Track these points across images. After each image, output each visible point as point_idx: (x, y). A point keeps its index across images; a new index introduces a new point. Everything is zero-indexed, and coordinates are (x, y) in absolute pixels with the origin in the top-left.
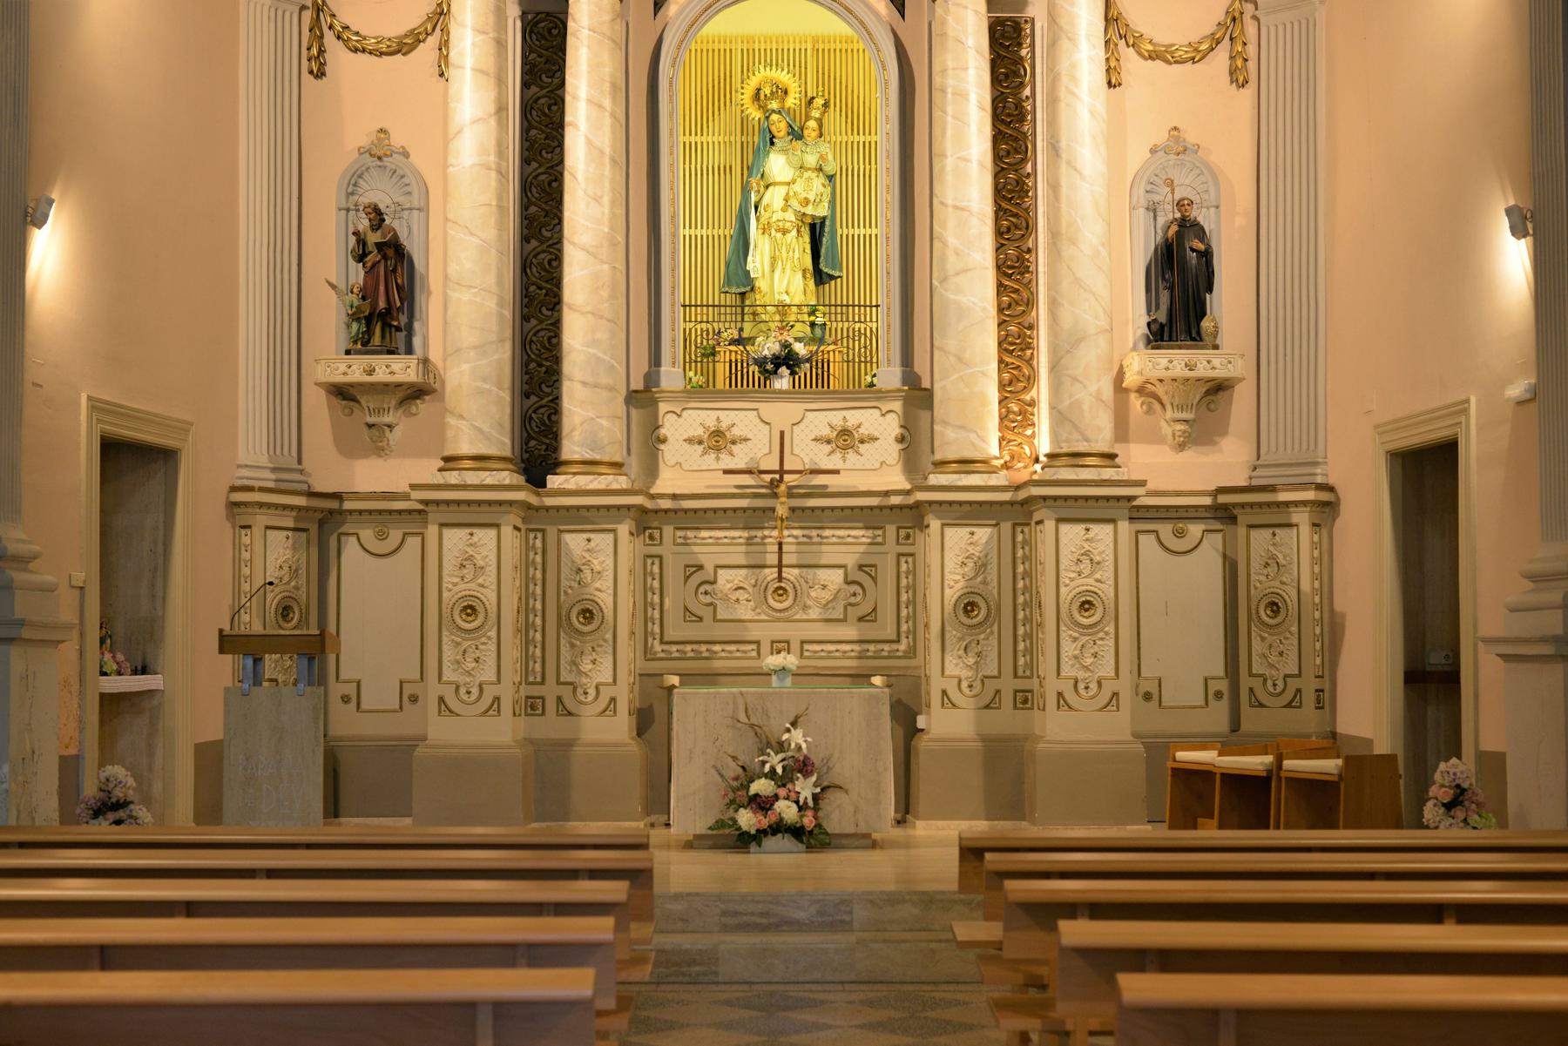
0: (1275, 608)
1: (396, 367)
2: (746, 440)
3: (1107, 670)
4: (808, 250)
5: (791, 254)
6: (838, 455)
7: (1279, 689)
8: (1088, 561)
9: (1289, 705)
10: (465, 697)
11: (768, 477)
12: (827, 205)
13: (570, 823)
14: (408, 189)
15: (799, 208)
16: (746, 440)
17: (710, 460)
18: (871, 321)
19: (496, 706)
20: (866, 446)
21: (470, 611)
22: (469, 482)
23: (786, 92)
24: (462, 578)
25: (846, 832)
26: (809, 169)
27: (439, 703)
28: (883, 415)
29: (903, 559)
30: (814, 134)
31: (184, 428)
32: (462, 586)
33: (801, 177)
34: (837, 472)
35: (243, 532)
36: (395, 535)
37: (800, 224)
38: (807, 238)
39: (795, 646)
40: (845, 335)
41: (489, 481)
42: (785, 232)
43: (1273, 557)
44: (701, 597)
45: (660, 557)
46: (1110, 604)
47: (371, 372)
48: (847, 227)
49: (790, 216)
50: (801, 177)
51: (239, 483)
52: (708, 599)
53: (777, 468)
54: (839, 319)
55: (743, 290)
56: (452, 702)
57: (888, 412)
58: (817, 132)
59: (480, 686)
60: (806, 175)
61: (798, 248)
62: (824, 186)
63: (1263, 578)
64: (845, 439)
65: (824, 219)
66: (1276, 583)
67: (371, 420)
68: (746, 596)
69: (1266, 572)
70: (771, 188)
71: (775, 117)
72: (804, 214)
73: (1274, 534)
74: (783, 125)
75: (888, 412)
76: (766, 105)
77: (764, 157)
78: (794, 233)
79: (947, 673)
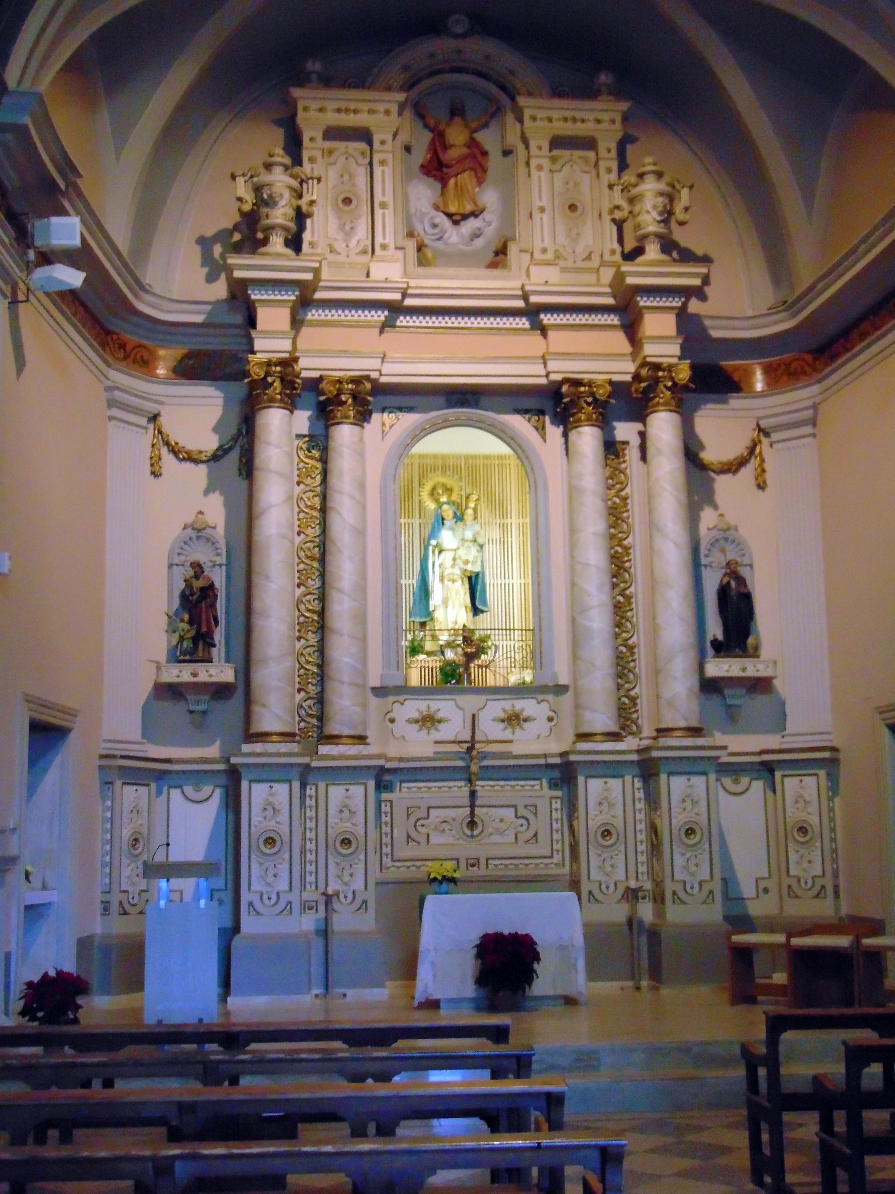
0: (804, 830)
4: (468, 594)
6: (509, 730)
8: (690, 801)
10: (803, 885)
14: (219, 551)
15: (462, 566)
18: (510, 640)
19: (288, 907)
20: (528, 723)
21: (346, 842)
22: (270, 751)
24: (684, 809)
25: (548, 994)
27: (249, 906)
28: (538, 703)
29: (554, 801)
30: (471, 518)
31: (72, 713)
33: (463, 546)
34: (511, 742)
35: (107, 786)
38: (467, 586)
39: (483, 862)
40: (509, 650)
42: (453, 581)
43: (801, 796)
45: (391, 802)
46: (286, 838)
47: (195, 675)
49: (457, 571)
50: (463, 546)
53: (469, 739)
54: (501, 638)
55: (423, 620)
57: (542, 701)
59: (278, 893)
60: (467, 544)
61: (460, 593)
63: (794, 810)
64: (513, 719)
66: (273, 823)
67: (192, 708)
68: (449, 827)
69: (340, 817)
71: (445, 507)
72: (466, 570)
73: (271, 787)
74: (451, 513)
75: (542, 701)
76: (439, 499)
79: (253, 888)
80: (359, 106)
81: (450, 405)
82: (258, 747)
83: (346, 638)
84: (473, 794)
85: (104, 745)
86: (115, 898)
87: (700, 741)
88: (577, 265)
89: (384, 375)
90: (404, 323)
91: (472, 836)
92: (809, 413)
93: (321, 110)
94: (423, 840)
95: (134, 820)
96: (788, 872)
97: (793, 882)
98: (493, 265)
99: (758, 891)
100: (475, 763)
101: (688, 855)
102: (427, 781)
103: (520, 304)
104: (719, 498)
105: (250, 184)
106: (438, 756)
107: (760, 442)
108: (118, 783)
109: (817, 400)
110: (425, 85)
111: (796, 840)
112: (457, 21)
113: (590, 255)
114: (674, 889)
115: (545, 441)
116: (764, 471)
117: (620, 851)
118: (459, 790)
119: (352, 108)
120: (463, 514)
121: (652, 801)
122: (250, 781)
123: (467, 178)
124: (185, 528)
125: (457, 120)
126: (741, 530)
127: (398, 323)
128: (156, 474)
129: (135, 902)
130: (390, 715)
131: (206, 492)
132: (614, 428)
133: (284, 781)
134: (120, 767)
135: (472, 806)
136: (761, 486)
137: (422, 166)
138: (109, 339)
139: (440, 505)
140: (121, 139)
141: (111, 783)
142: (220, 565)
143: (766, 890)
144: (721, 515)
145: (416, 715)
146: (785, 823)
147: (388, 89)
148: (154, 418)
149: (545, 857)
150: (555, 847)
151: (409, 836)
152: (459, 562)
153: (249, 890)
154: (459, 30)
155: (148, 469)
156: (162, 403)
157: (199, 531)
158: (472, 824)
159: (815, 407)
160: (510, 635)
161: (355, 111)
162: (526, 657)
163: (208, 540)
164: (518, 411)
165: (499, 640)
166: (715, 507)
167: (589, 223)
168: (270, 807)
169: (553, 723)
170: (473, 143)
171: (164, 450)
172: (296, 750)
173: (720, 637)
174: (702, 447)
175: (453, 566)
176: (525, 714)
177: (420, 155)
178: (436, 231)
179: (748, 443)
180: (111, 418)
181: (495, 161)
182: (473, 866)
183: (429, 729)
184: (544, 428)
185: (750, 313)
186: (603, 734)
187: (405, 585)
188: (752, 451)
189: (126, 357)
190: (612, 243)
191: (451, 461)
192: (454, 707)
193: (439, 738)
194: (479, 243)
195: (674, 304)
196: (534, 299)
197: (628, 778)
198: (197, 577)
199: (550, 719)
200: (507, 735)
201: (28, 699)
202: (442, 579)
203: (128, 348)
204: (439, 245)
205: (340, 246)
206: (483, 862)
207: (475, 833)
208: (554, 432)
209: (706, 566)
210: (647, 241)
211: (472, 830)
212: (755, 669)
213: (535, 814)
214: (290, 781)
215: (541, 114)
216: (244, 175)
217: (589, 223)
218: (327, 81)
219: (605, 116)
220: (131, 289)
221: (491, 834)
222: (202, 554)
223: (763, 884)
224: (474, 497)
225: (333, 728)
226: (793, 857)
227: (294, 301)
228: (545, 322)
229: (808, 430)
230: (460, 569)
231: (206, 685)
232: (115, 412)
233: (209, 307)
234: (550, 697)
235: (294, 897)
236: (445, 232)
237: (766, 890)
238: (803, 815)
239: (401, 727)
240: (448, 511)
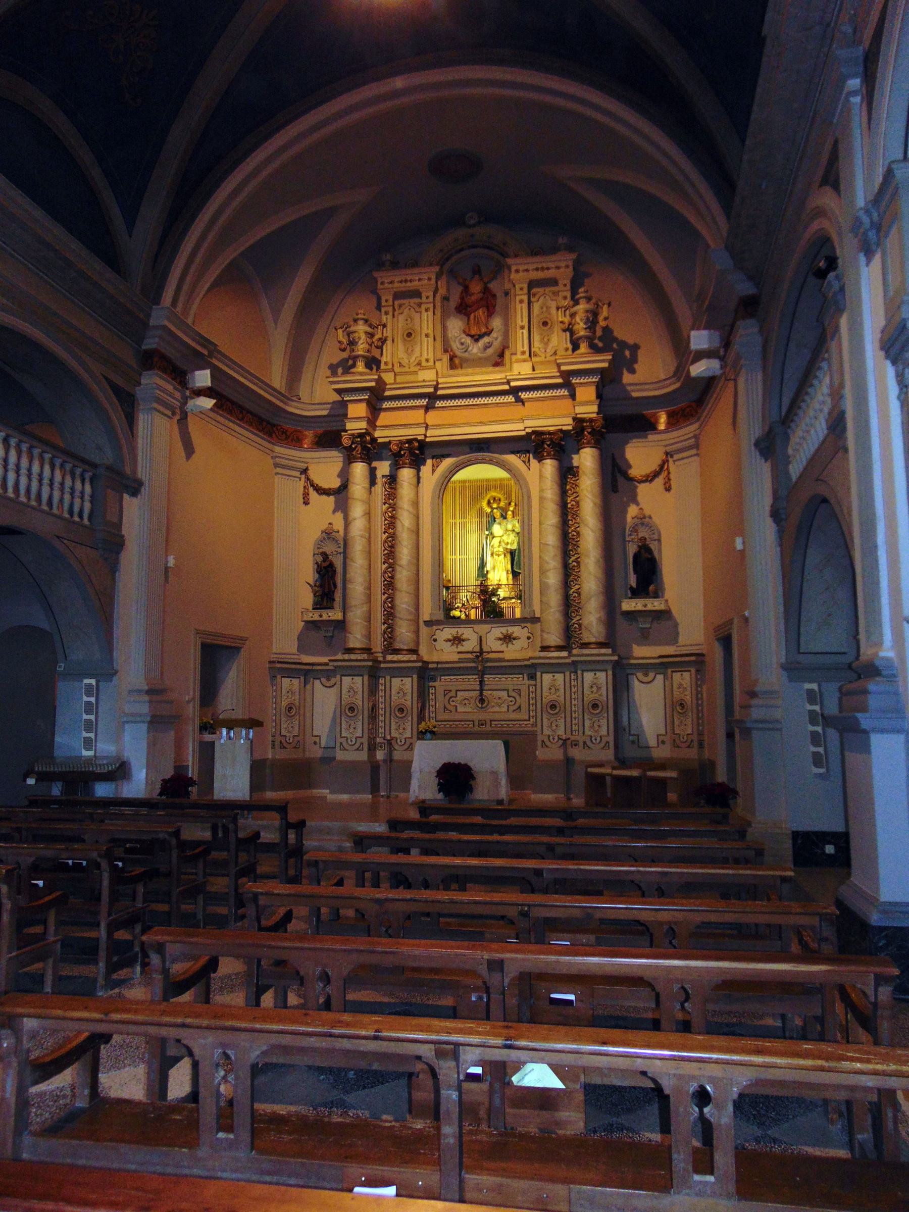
1: (656, 604)
2: (469, 640)
3: (604, 731)
6: (505, 645)
7: (354, 742)
9: (357, 749)
10: (350, 743)
11: (475, 654)
13: (314, 791)
16: (469, 640)
17: (454, 648)
21: (553, 707)
23: (500, 500)
32: (591, 696)
36: (651, 675)
41: (359, 658)
42: (499, 555)
43: (352, 688)
44: (452, 703)
45: (435, 687)
46: (409, 709)
47: (645, 606)
49: (501, 549)
51: (272, 660)
52: (454, 704)
56: (589, 743)
64: (508, 639)
65: (515, 550)
71: (495, 511)
73: (595, 674)
78: (503, 556)
80: (413, 277)
81: (472, 451)
82: (396, 657)
83: (404, 594)
84: (481, 682)
85: (272, 656)
86: (278, 739)
88: (547, 359)
90: (440, 405)
91: (482, 708)
92: (692, 441)
93: (391, 283)
94: (453, 710)
95: (290, 696)
96: (341, 733)
98: (496, 364)
99: (658, 743)
101: (552, 719)
102: (462, 675)
103: (506, 387)
104: (640, 498)
105: (345, 333)
106: (461, 661)
107: (668, 461)
108: (279, 677)
109: (697, 432)
110: (454, 259)
111: (397, 716)
112: (471, 217)
113: (555, 352)
116: (669, 479)
118: (472, 681)
119: (409, 279)
120: (506, 514)
121: (373, 690)
122: (542, 673)
123: (481, 313)
125: (477, 276)
126: (654, 519)
127: (436, 406)
128: (306, 503)
129: (291, 741)
130: (434, 637)
131: (334, 512)
132: (572, 459)
133: (603, 670)
134: (279, 668)
135: (481, 690)
136: (668, 489)
137: (456, 308)
138: (275, 429)
139: (493, 509)
140: (276, 313)
141: (276, 677)
142: (340, 553)
143: (663, 742)
144: (641, 509)
145: (450, 637)
147: (431, 265)
148: (305, 471)
149: (525, 720)
150: (531, 714)
151: (445, 708)
152: (503, 544)
153: (584, 733)
154: (472, 222)
155: (302, 501)
156: (307, 463)
157: (329, 534)
158: (482, 701)
159: (695, 436)
161: (411, 281)
163: (334, 539)
164: (513, 453)
166: (637, 504)
167: (555, 333)
168: (553, 687)
169: (531, 640)
170: (486, 290)
171: (311, 489)
173: (634, 585)
174: (630, 467)
175: (499, 546)
177: (454, 302)
178: (464, 347)
179: (659, 462)
180: (277, 474)
181: (500, 300)
182: (482, 725)
183: (507, 644)
184: (529, 461)
185: (664, 377)
186: (407, 650)
188: (661, 467)
189: (286, 439)
190: (566, 344)
191: (506, 482)
192: (472, 632)
194: (490, 351)
195: (594, 380)
196: (513, 384)
197: (567, 674)
198: (324, 561)
199: (435, 640)
200: (503, 648)
201: (198, 632)
202: (492, 555)
203: (288, 433)
204: (466, 355)
205: (405, 362)
206: (488, 722)
207: (484, 705)
208: (534, 462)
209: (629, 541)
210: (580, 341)
211: (482, 704)
213: (520, 695)
214: (606, 671)
215: (521, 268)
216: (341, 328)
217: (555, 333)
218: (395, 265)
219: (563, 264)
220: (282, 402)
221: (493, 706)
222: (329, 548)
223: (661, 738)
225: (398, 645)
226: (676, 722)
227: (598, 382)
228: (522, 397)
229: (694, 452)
230: (503, 548)
231: (650, 611)
232: (279, 470)
233: (329, 406)
234: (529, 625)
236: (469, 347)
237: (663, 742)
238: (554, 697)
239: (441, 644)
240: (497, 513)
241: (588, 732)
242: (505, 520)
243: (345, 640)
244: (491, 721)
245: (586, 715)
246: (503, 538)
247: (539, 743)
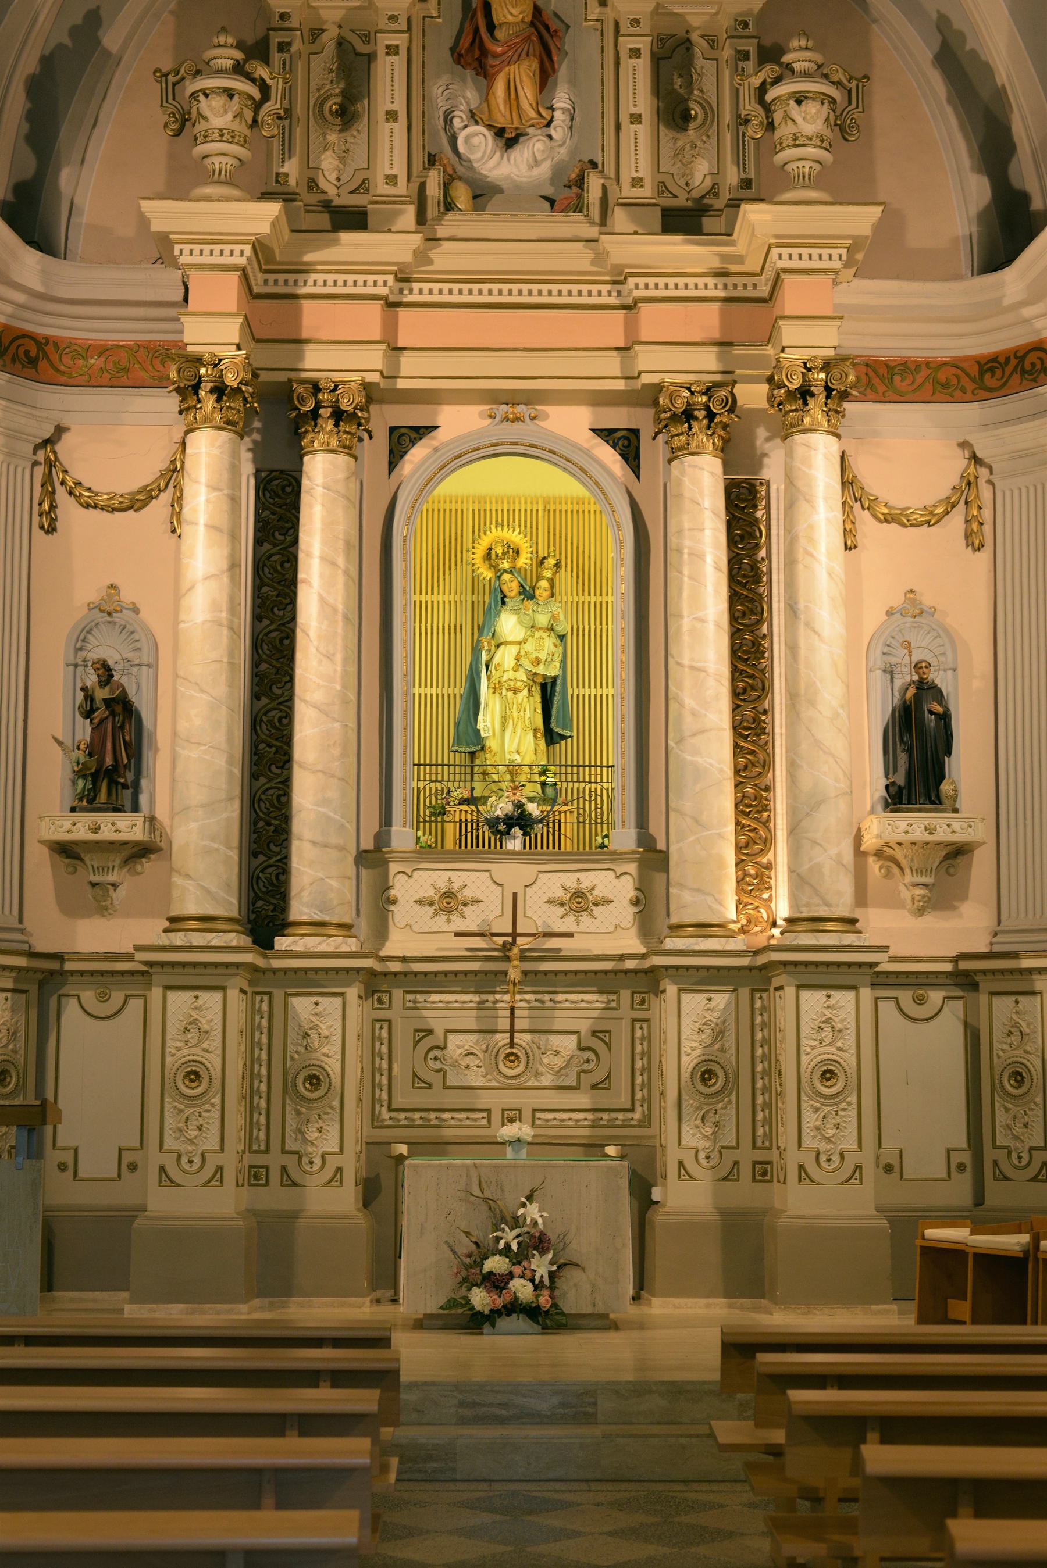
0: (1019, 1078)
2: (478, 901)
4: (539, 710)
5: (522, 713)
6: (571, 918)
8: (829, 1029)
12: (558, 665)
15: (530, 667)
16: (478, 901)
19: (218, 1176)
22: (195, 944)
24: (186, 1043)
26: (541, 629)
28: (618, 877)
30: (546, 594)
32: (186, 1051)
34: (570, 935)
36: (117, 997)
37: (531, 683)
38: (538, 698)
42: (516, 691)
43: (1016, 1025)
44: (431, 1063)
45: (389, 1021)
46: (217, 1074)
47: (96, 830)
48: (578, 687)
49: (522, 676)
52: (438, 1065)
55: (473, 749)
58: (548, 593)
60: (538, 634)
61: (530, 708)
62: (556, 646)
63: (1006, 1047)
65: (555, 678)
70: (502, 647)
71: (506, 577)
72: (535, 674)
73: (1017, 1002)
74: (515, 585)
76: (498, 565)
77: (496, 616)
78: (525, 692)
79: (684, 1143)
87: (849, 939)
89: (376, 371)
97: (1001, 1156)
100: (515, 967)
114: (161, 1163)
115: (638, 478)
117: (730, 1102)
124: (889, 613)
146: (992, 1068)
160: (578, 774)
162: (601, 808)
165: (572, 781)
172: (234, 943)
176: (468, 893)
187: (420, 695)
193: (463, 928)
206: (527, 1114)
212: (113, 829)
224: (551, 562)
235: (230, 1162)
238: (829, 1052)
241: (808, 1142)
242: (530, 604)
243: (166, 892)
244: (534, 1110)
245: (167, 1099)
246: (529, 647)
247: (672, 1170)
